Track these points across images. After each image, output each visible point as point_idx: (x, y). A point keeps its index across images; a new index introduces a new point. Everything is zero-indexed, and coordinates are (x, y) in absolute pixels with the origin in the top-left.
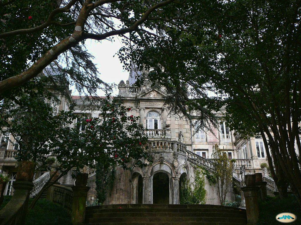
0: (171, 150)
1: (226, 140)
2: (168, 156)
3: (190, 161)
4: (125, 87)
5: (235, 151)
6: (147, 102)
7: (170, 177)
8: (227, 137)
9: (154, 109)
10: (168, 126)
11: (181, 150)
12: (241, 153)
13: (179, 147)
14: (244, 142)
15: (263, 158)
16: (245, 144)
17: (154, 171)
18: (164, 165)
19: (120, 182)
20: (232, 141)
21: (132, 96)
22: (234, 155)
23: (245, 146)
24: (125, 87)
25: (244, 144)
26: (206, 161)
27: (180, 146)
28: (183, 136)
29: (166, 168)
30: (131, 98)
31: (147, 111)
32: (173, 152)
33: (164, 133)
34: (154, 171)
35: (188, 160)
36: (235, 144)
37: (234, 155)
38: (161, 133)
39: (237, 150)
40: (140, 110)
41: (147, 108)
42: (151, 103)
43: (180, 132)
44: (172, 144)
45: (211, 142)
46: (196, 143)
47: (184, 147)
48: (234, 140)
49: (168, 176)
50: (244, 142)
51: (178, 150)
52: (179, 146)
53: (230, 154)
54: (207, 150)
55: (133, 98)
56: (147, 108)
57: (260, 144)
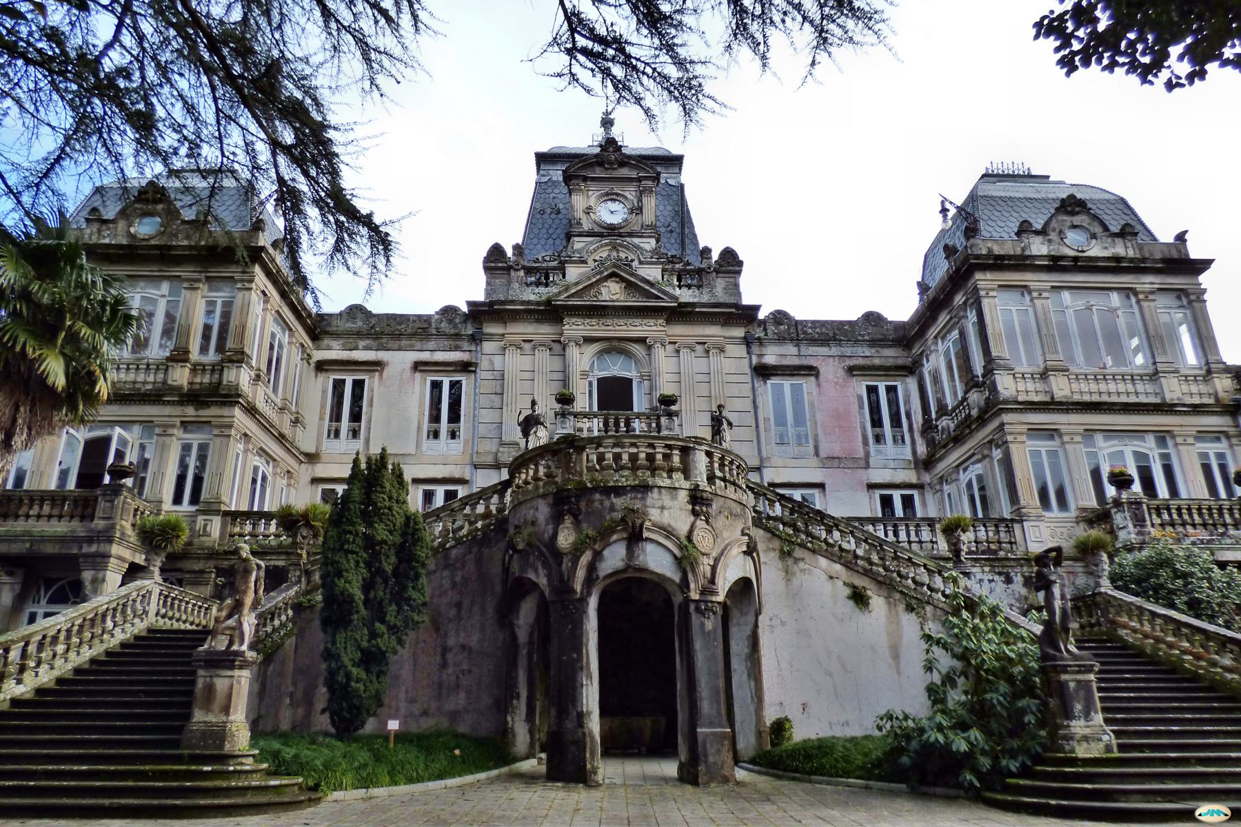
0: (678, 476)
1: (889, 448)
2: (668, 510)
3: (767, 529)
4: (509, 268)
5: (927, 487)
6: (590, 317)
7: (678, 599)
8: (895, 441)
9: (616, 343)
10: (668, 401)
11: (724, 479)
12: (955, 495)
13: (716, 465)
14: (974, 454)
15: (1065, 515)
16: (979, 461)
17: (602, 574)
18: (649, 547)
19: (460, 619)
20: (914, 452)
21: (532, 298)
22: (924, 504)
23: (976, 469)
24: (509, 268)
25: (973, 463)
26: (837, 526)
27: (722, 459)
28: (730, 424)
29: (657, 560)
30: (529, 303)
31: (593, 348)
32: (687, 485)
33: (654, 425)
34: (602, 574)
35: (757, 522)
36: (927, 464)
37: (924, 504)
38: (643, 425)
39: (938, 487)
40: (564, 349)
41: (589, 340)
42: (603, 321)
43: (720, 406)
44: (685, 451)
45: (833, 458)
46: (776, 461)
47: (738, 467)
48: (922, 449)
49: (668, 602)
50: (974, 454)
51: (711, 479)
52: (716, 459)
53: (908, 502)
54: (821, 486)
55: (538, 303)
56: (589, 340)
57: (1032, 457)
